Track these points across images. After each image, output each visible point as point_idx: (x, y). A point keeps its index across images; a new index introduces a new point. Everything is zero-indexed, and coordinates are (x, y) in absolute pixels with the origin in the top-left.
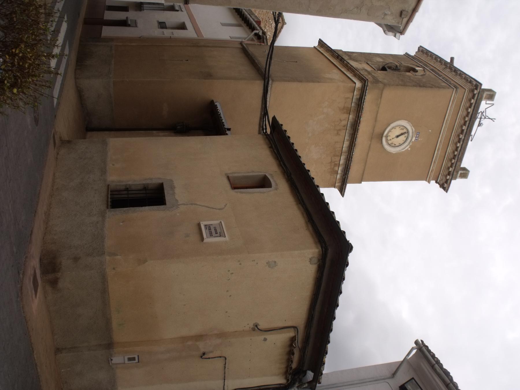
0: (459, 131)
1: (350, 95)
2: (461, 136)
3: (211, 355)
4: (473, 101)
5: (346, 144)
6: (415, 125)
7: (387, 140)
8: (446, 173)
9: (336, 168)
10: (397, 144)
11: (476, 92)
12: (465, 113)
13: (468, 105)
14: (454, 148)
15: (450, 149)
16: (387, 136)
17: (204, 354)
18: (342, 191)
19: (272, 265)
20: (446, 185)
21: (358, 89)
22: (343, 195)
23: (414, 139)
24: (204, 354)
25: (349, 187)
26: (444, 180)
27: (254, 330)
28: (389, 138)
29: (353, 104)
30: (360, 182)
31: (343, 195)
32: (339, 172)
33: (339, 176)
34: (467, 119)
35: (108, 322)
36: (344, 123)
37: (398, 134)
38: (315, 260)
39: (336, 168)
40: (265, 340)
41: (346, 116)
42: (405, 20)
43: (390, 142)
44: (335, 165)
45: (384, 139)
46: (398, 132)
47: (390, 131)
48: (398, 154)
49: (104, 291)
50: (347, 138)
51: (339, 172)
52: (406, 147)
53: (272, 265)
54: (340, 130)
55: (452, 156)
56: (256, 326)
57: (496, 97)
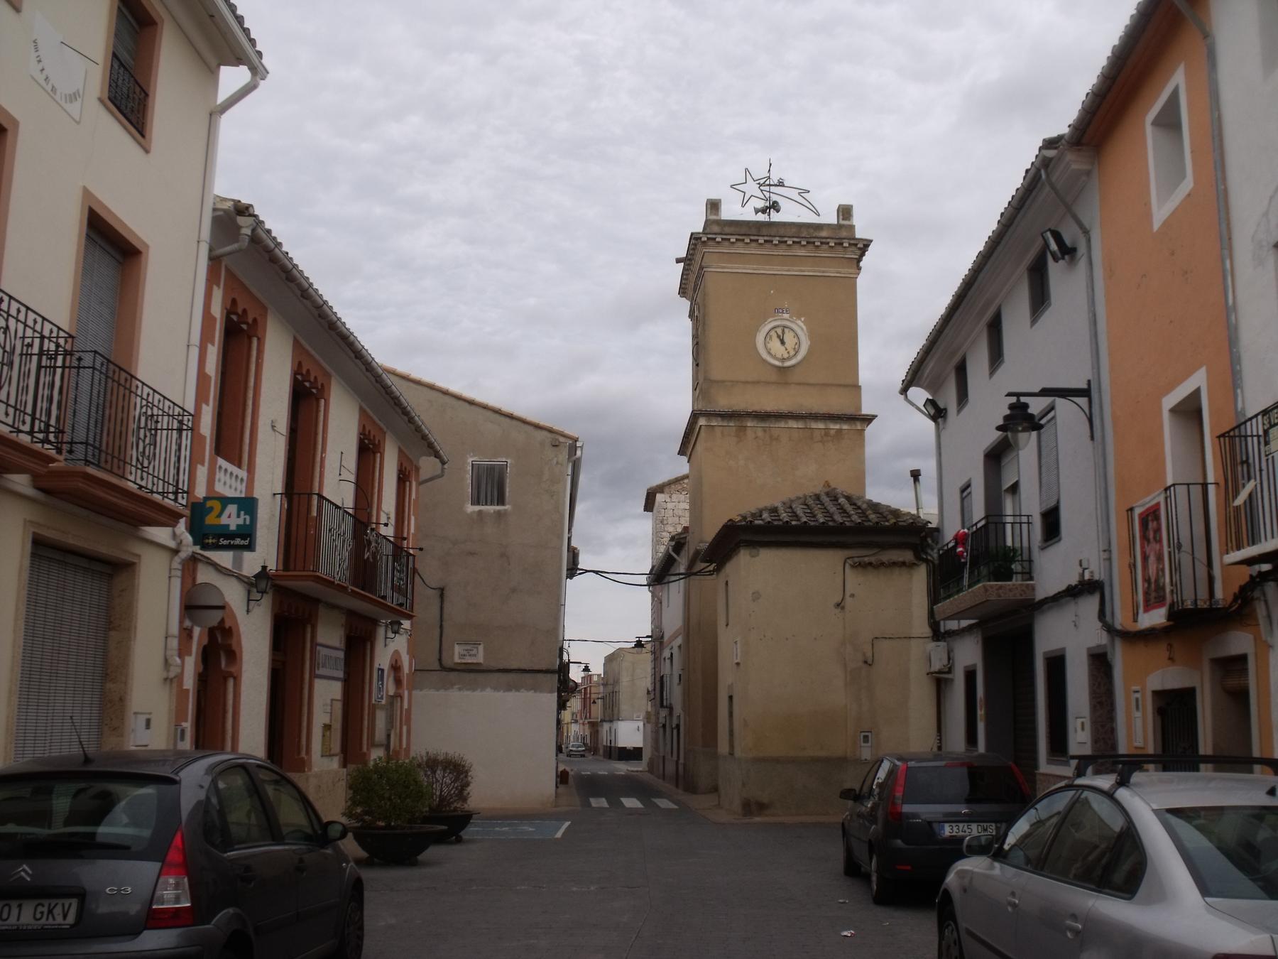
0: (767, 245)
1: (718, 431)
2: (776, 242)
3: (869, 654)
4: (719, 239)
5: (793, 424)
6: (764, 318)
7: (789, 359)
8: (839, 248)
9: (832, 432)
10: (796, 340)
11: (704, 239)
12: (740, 244)
13: (726, 243)
14: (797, 246)
15: (802, 252)
16: (783, 360)
17: (866, 662)
18: (869, 419)
19: (756, 596)
20: (860, 245)
21: (709, 420)
22: (874, 417)
23: (786, 316)
24: (866, 662)
25: (865, 411)
26: (853, 248)
27: (843, 608)
28: (786, 356)
29: (732, 424)
30: (859, 387)
31: (874, 417)
32: (837, 427)
33: (845, 427)
34: (747, 240)
35: (816, 760)
36: (760, 433)
37: (778, 343)
38: (754, 551)
39: (832, 432)
40: (852, 596)
41: (749, 432)
42: (562, 439)
43: (792, 353)
44: (827, 434)
45: (787, 364)
46: (775, 344)
47: (774, 357)
48: (812, 336)
49: (777, 760)
50: (782, 424)
51: (837, 427)
52: (800, 326)
53: (756, 596)
54: (771, 437)
55: (811, 247)
56: (838, 605)
57: (714, 197)
